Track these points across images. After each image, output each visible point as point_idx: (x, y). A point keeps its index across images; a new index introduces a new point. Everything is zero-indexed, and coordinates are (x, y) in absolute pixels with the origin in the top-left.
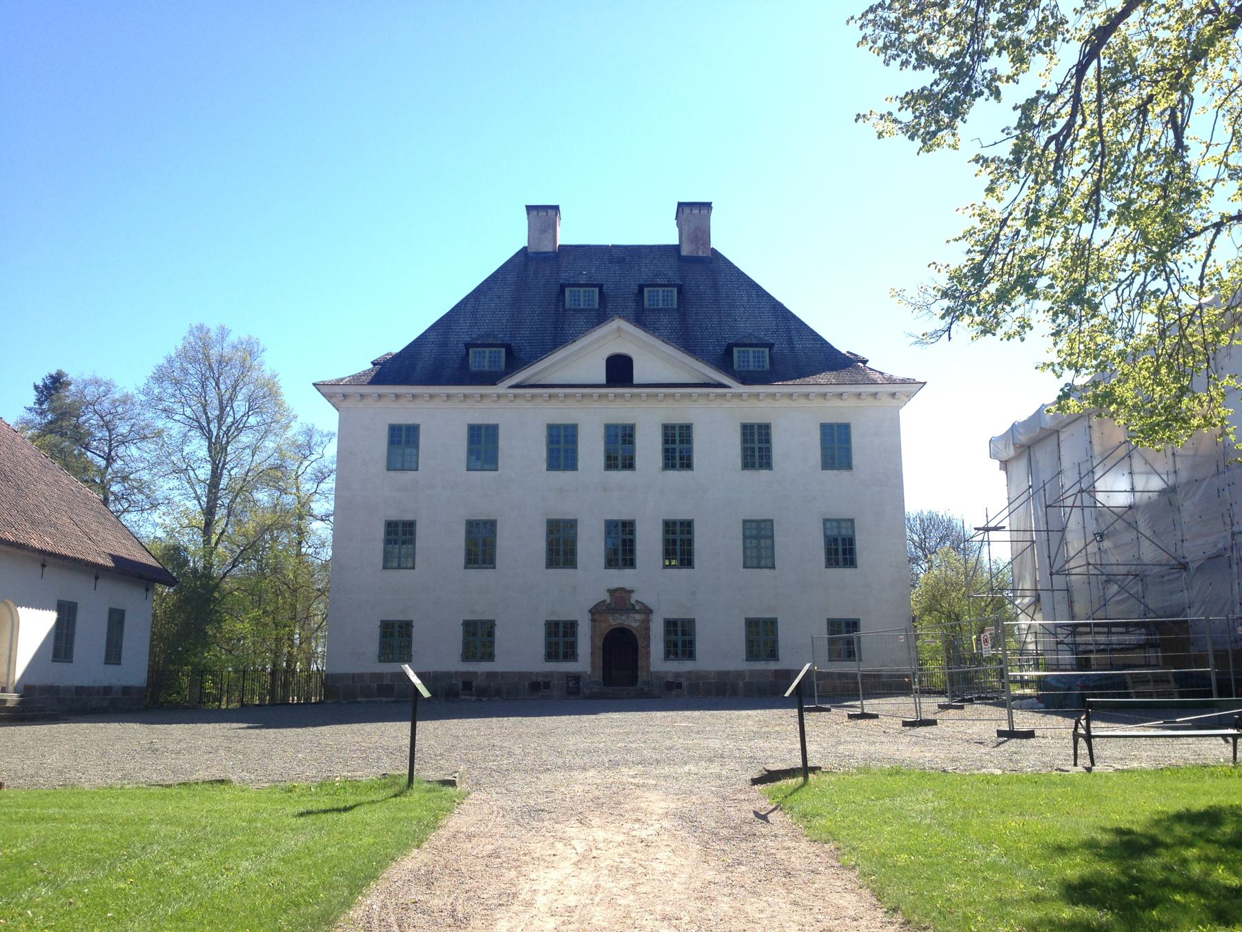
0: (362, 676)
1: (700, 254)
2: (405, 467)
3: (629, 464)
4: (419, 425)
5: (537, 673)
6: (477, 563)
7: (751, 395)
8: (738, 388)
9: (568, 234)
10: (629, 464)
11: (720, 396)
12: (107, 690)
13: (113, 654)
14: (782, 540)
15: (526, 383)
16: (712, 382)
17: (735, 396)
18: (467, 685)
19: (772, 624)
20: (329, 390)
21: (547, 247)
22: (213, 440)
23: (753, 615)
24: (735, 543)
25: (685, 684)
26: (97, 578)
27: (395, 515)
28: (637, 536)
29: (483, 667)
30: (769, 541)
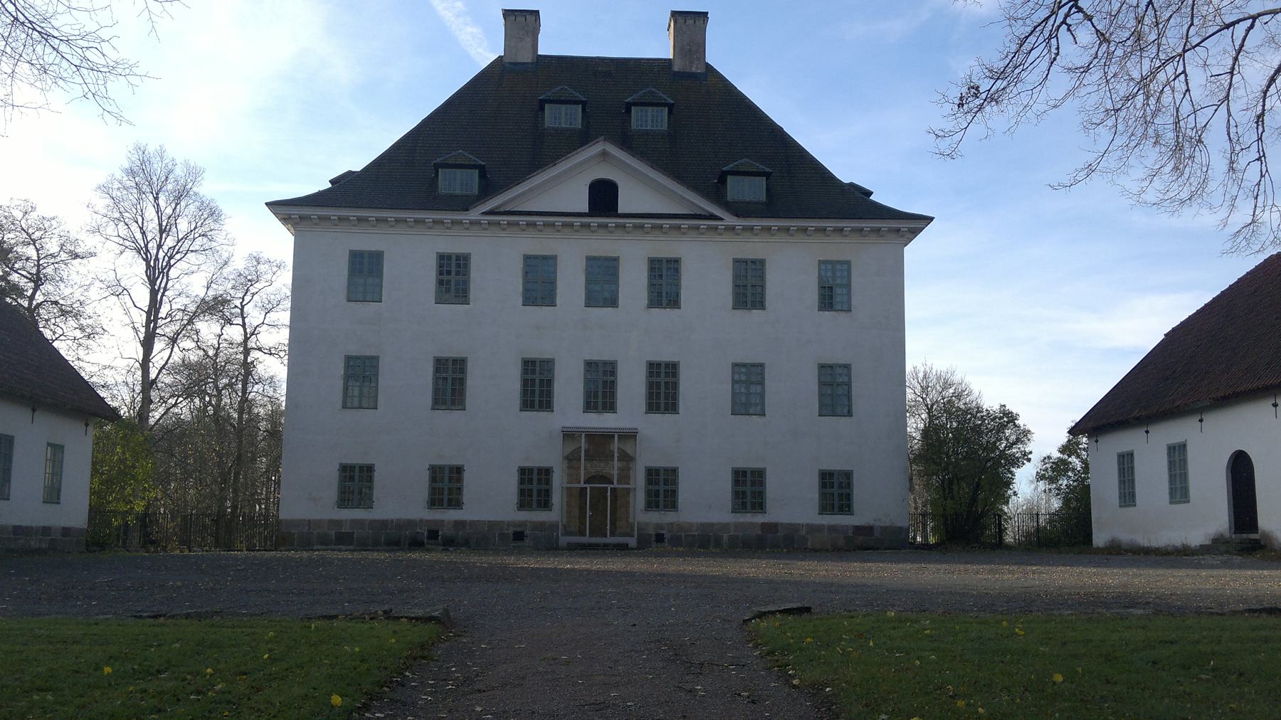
0: (318, 523)
1: (694, 70)
2: (368, 299)
3: (612, 302)
4: (383, 251)
5: (509, 522)
6: (445, 404)
7: (745, 229)
8: (730, 220)
9: (549, 45)
10: (612, 302)
11: (802, 229)
12: (46, 530)
13: (53, 495)
14: (474, 381)
15: (502, 210)
16: (703, 213)
17: (731, 229)
18: (433, 534)
19: (368, 470)
20: (284, 209)
21: (526, 57)
22: (152, 264)
23: (741, 464)
24: (513, 384)
25: (667, 536)
26: (34, 410)
27: (355, 350)
28: (618, 377)
29: (452, 515)
30: (759, 388)
